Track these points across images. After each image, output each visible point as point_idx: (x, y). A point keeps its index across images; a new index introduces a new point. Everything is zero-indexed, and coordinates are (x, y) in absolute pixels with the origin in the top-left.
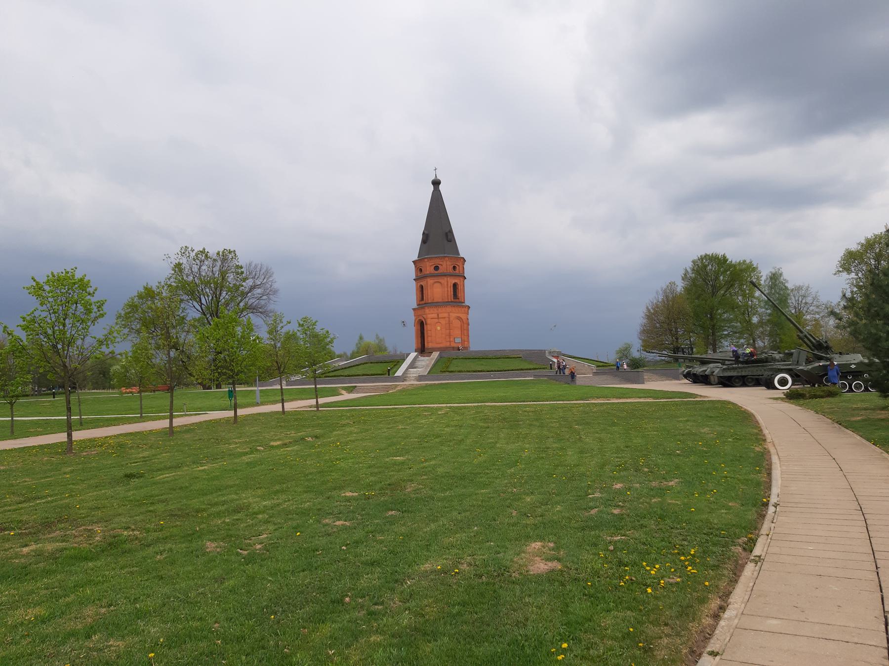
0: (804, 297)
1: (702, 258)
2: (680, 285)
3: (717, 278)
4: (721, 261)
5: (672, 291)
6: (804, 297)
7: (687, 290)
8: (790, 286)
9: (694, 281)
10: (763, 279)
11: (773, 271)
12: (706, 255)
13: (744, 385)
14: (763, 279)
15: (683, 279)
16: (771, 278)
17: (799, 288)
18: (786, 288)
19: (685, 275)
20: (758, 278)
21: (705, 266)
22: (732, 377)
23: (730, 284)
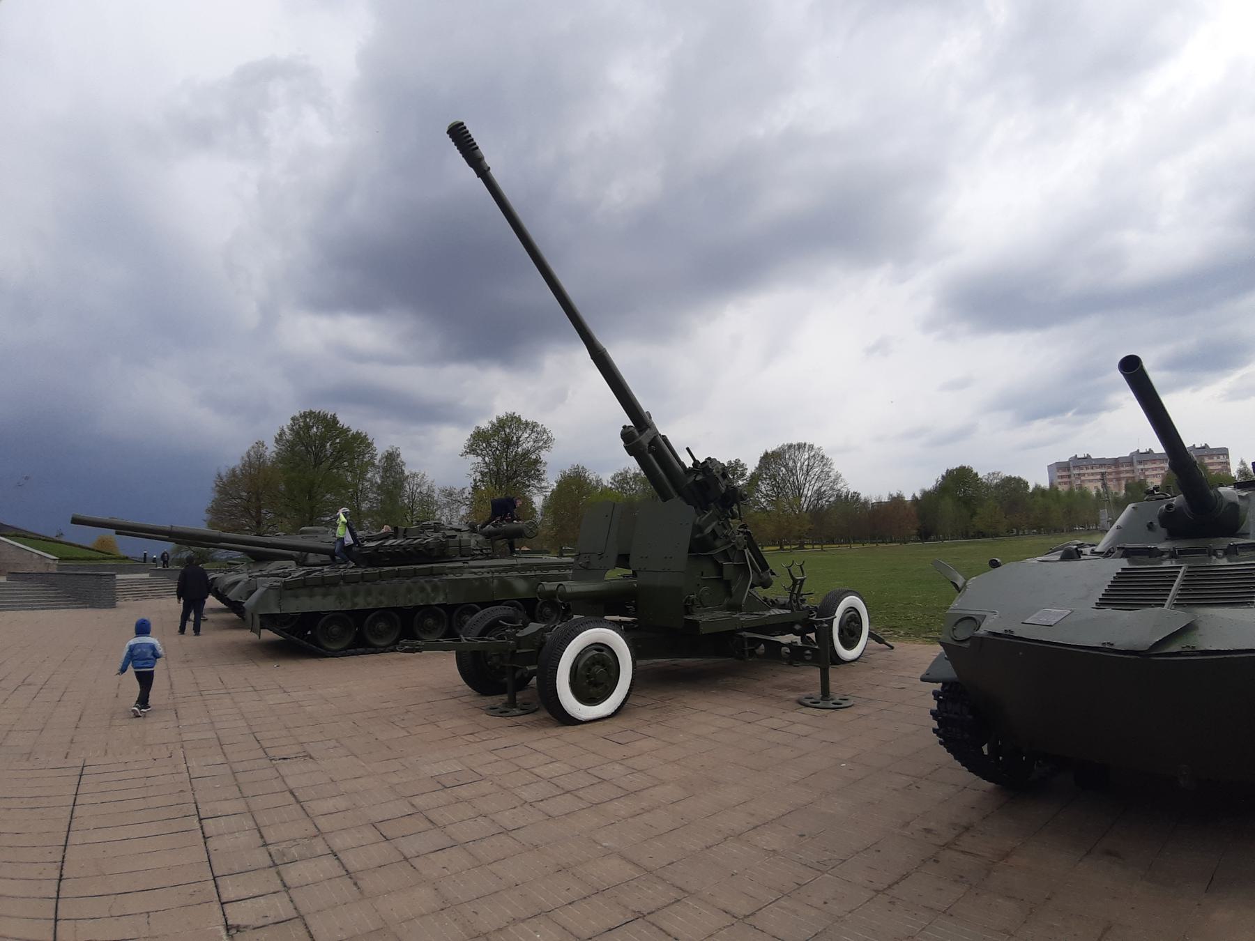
0: (419, 485)
1: (304, 416)
2: (271, 449)
3: (323, 446)
4: (330, 424)
6: (419, 485)
8: (407, 473)
9: (291, 446)
10: (379, 457)
12: (311, 413)
14: (379, 457)
15: (277, 441)
17: (415, 475)
18: (403, 472)
19: (280, 435)
20: (373, 457)
21: (308, 427)
22: (317, 615)
23: (338, 456)
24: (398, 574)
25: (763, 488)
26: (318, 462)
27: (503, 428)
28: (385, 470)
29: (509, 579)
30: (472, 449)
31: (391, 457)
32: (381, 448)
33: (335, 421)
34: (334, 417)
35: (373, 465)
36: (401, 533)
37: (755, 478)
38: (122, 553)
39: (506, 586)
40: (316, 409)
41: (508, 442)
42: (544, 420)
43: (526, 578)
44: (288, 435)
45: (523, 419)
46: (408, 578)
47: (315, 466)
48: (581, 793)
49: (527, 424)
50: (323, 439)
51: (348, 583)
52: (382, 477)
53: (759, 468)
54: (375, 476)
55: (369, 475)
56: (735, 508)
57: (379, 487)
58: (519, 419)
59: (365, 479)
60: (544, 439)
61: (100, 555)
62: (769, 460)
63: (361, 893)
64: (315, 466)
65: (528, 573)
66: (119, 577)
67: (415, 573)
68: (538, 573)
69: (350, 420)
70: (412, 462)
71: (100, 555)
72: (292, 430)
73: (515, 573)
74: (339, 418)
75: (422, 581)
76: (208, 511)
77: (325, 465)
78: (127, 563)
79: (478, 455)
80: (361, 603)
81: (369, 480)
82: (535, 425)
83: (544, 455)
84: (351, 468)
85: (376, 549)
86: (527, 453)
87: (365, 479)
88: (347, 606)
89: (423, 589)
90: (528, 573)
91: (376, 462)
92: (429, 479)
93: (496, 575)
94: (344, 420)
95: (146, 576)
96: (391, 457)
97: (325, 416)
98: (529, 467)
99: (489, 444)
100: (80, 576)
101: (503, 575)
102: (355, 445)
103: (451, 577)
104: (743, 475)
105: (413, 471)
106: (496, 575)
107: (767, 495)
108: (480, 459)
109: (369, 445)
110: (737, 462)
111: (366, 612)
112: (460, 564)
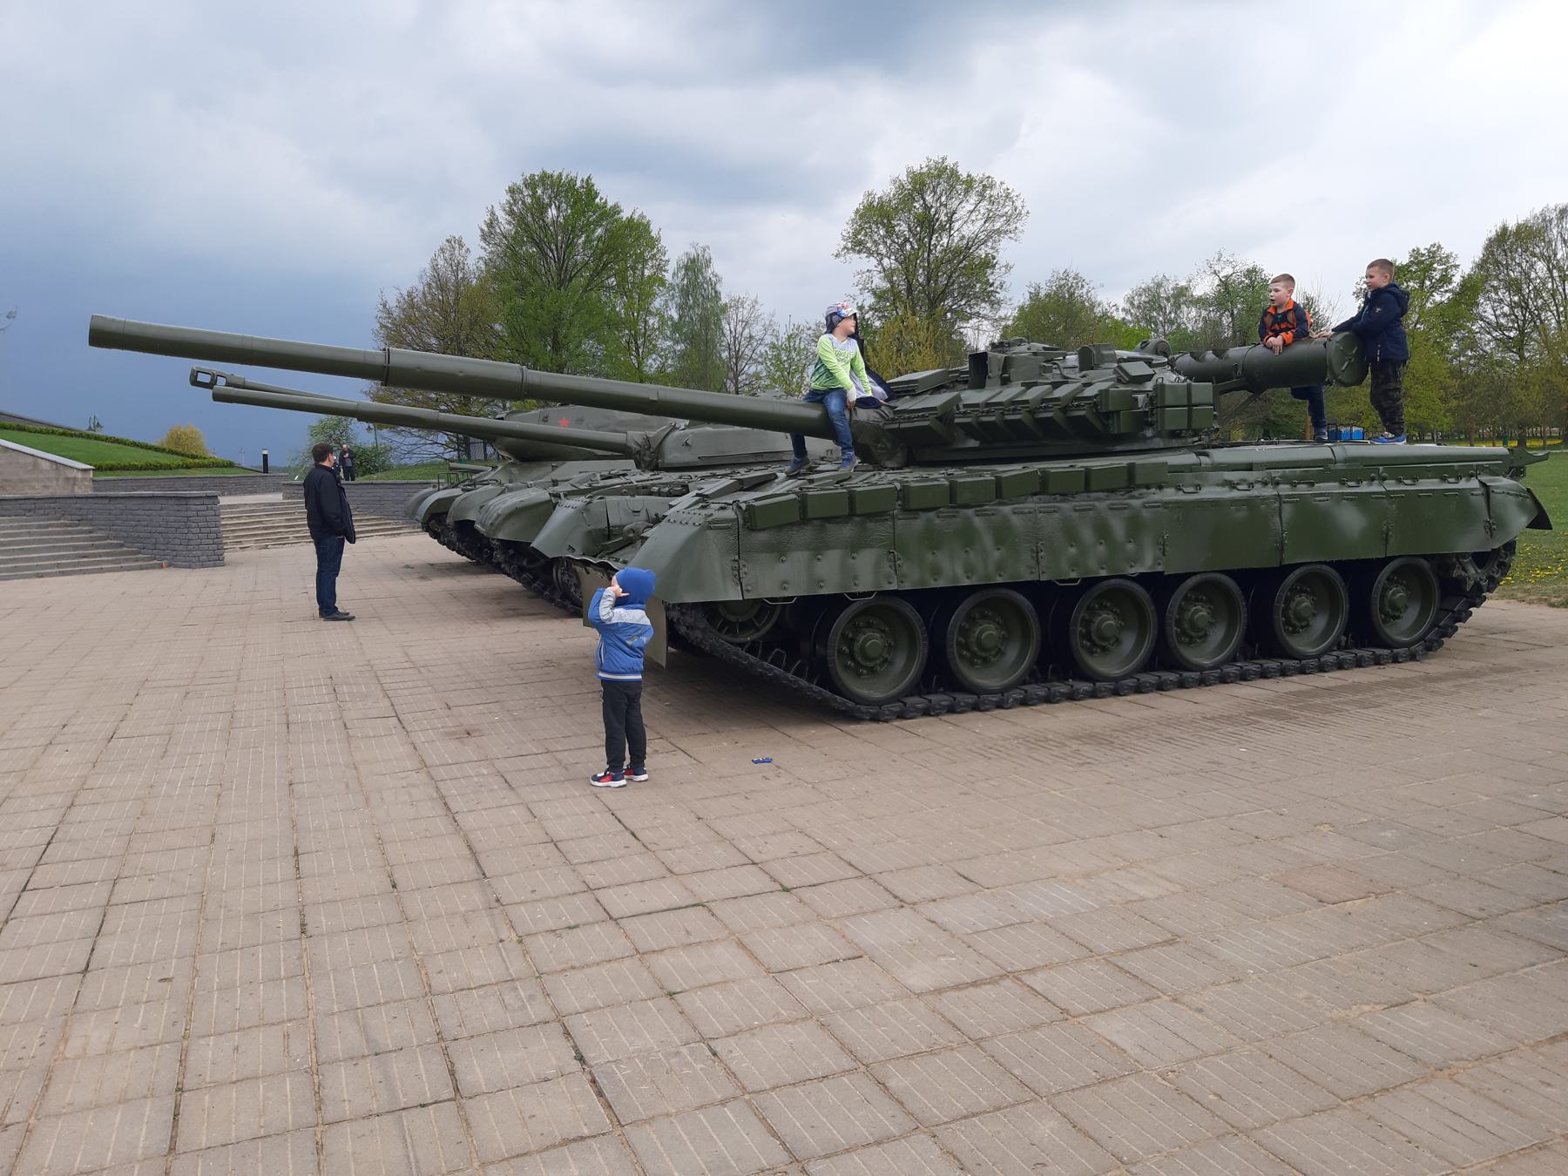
0: (747, 324)
1: (531, 184)
2: (476, 255)
3: (570, 244)
4: (582, 198)
5: (458, 267)
6: (747, 324)
7: (495, 273)
8: (724, 300)
10: (672, 267)
11: (693, 253)
13: (941, 687)
14: (672, 267)
15: (484, 237)
16: (687, 268)
17: (738, 303)
19: (490, 225)
20: (660, 268)
21: (542, 208)
24: (1043, 486)
25: (1487, 310)
26: (564, 280)
27: (922, 194)
28: (685, 292)
29: (1324, 504)
30: (857, 244)
31: (694, 267)
32: (674, 248)
33: (591, 193)
34: (588, 184)
35: (662, 282)
36: (994, 370)
37: (1470, 290)
38: (220, 456)
39: (1312, 518)
40: (553, 170)
41: (928, 224)
42: (1005, 172)
43: (1361, 500)
44: (505, 224)
45: (963, 174)
46: (1065, 496)
47: (561, 283)
48: (1037, 981)
49: (969, 183)
50: (570, 229)
51: (910, 511)
52: (680, 307)
53: (1481, 265)
54: (666, 305)
55: (657, 303)
56: (1390, 370)
57: (676, 327)
58: (954, 174)
59: (649, 313)
60: (1004, 212)
61: (178, 460)
62: (1505, 243)
63: (302, 914)
64: (561, 283)
65: (1365, 488)
66: (224, 500)
67: (1088, 481)
68: (1391, 485)
69: (621, 194)
70: (733, 280)
71: (178, 460)
72: (511, 213)
73: (1332, 487)
74: (598, 184)
75: (1101, 503)
76: (911, 173)
77: (580, 281)
78: (230, 473)
79: (870, 254)
80: (953, 570)
81: (659, 314)
82: (987, 185)
83: (1005, 251)
84: (621, 290)
85: (945, 416)
86: (962, 252)
87: (649, 313)
88: (912, 578)
89: (1103, 532)
90: (1365, 488)
91: (668, 277)
92: (764, 311)
93: (1284, 489)
94: (610, 191)
95: (277, 497)
96: (694, 267)
97: (572, 182)
98: (968, 273)
99: (890, 230)
100: (146, 508)
101: (1302, 489)
102: (630, 239)
103: (1169, 494)
104: (1446, 279)
105: (736, 295)
106: (1284, 489)
107: (1499, 327)
108: (873, 261)
109: (653, 243)
110: (1434, 253)
111: (955, 594)
112: (1189, 458)
